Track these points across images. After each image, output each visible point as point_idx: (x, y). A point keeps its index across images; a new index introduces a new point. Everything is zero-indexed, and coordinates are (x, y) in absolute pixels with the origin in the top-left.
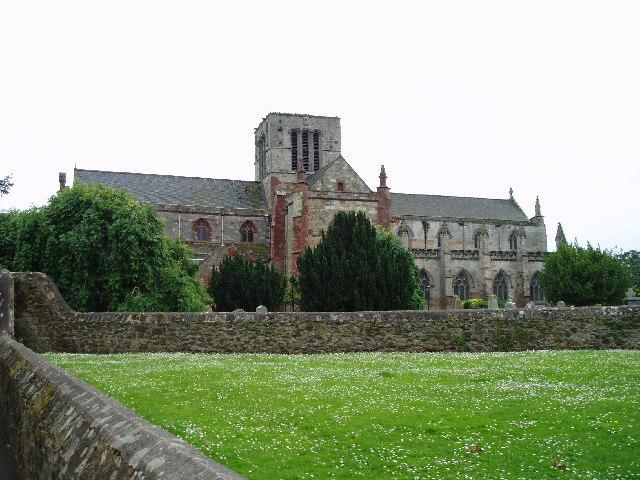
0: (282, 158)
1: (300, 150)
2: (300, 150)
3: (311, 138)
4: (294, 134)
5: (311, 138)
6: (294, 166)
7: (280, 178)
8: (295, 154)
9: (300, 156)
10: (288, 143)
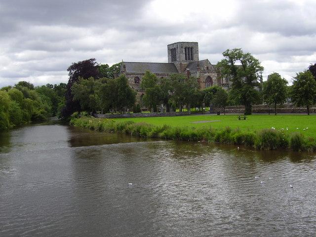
1: (187, 54)
2: (187, 54)
3: (187, 58)
4: (185, 49)
5: (187, 58)
6: (186, 59)
8: (186, 54)
9: (187, 56)
10: (184, 52)
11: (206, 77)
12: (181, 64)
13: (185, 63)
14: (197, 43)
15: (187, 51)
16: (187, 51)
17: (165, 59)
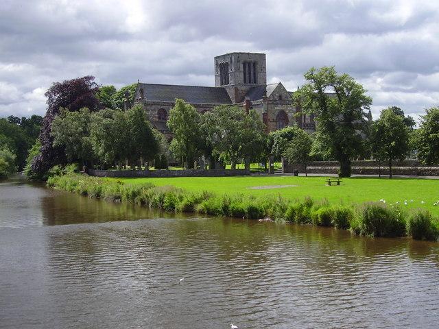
0: (236, 78)
1: (252, 75)
2: (252, 75)
3: (252, 65)
4: (244, 64)
5: (252, 65)
7: (239, 88)
8: (245, 74)
10: (242, 69)
11: (277, 113)
12: (236, 90)
13: (244, 88)
14: (264, 55)
15: (247, 68)
16: (247, 68)
17: (210, 81)
